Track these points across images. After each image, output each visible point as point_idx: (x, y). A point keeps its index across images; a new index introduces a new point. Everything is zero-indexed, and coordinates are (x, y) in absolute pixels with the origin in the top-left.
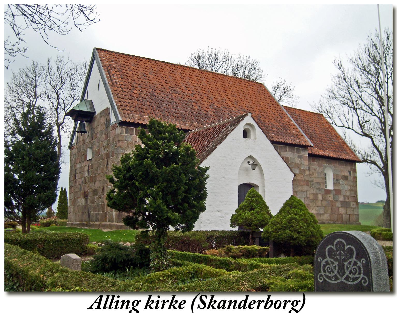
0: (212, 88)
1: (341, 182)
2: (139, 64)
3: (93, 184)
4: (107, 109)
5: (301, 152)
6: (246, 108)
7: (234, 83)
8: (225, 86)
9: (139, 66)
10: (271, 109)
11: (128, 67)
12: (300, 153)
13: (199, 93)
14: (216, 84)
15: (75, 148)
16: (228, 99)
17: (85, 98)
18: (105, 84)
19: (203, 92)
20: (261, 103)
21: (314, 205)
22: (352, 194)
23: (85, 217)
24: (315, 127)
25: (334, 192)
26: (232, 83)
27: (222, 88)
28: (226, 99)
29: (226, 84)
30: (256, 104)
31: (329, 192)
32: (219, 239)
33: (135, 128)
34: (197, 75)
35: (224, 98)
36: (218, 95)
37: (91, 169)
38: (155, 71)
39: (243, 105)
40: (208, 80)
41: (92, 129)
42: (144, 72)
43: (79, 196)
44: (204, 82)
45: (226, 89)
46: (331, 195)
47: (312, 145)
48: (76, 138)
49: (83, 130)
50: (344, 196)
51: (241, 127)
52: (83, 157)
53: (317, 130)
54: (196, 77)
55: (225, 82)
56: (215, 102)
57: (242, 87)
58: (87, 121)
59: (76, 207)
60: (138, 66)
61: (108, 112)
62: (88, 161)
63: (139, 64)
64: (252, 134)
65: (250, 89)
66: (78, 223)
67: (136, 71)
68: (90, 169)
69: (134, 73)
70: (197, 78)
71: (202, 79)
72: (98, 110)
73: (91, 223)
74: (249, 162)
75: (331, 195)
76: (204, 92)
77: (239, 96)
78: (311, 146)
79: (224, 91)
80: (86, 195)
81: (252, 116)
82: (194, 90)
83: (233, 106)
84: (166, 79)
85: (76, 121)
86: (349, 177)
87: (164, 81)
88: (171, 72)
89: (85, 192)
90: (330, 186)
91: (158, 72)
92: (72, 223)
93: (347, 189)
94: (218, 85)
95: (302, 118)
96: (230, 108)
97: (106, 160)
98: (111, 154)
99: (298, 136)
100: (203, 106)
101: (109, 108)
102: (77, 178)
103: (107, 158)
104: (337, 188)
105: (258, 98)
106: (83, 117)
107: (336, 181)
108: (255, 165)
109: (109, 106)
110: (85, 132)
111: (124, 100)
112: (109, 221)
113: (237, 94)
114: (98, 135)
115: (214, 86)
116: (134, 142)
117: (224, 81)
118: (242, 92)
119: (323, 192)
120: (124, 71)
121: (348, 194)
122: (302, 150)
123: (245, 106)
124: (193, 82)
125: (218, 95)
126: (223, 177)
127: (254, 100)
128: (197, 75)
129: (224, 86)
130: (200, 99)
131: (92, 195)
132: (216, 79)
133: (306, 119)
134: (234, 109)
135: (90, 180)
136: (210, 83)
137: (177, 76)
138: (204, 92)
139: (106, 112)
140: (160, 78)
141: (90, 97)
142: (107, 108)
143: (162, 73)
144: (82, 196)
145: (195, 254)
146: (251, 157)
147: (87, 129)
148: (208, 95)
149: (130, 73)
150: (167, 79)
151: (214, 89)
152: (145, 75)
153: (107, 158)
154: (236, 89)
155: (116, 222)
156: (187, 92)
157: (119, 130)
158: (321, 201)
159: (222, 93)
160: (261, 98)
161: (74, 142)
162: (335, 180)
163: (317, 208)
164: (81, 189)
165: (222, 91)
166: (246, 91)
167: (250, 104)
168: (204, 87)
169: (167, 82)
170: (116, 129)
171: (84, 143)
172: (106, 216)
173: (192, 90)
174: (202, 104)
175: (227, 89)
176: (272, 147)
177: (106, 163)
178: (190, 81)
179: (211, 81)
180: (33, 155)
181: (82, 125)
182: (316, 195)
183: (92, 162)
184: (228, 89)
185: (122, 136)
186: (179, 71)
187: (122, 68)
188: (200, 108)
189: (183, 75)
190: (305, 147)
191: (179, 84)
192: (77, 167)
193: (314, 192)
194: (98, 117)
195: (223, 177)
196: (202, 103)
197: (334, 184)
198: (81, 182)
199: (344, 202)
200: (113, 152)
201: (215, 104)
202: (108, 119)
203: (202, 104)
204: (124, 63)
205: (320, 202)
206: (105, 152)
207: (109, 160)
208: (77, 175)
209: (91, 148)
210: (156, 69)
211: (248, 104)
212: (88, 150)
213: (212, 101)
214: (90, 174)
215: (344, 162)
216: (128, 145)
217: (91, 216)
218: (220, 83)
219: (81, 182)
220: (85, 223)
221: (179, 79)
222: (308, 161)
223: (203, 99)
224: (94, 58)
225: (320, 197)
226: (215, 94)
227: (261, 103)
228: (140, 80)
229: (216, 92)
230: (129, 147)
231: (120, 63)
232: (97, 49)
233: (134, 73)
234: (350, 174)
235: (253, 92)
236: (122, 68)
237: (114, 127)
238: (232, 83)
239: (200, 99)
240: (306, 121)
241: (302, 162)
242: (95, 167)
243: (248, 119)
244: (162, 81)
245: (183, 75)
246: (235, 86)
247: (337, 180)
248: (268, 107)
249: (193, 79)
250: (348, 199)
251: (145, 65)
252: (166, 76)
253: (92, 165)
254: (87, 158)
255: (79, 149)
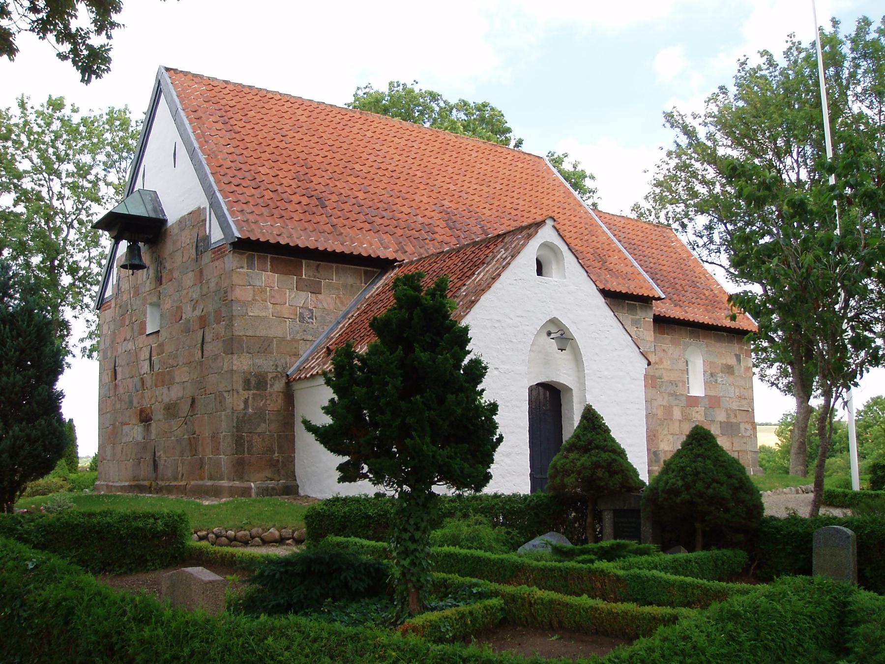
0: (434, 166)
1: (720, 380)
2: (266, 106)
3: (165, 390)
4: (199, 211)
5: (639, 311)
6: (514, 212)
7: (482, 156)
8: (462, 162)
9: (267, 111)
10: (568, 214)
11: (241, 112)
12: (636, 314)
13: (407, 177)
14: (443, 157)
15: (113, 305)
16: (471, 191)
17: (138, 186)
18: (192, 154)
19: (417, 173)
20: (544, 201)
21: (665, 432)
22: (743, 406)
23: (145, 470)
24: (659, 256)
25: (706, 402)
26: (476, 154)
27: (457, 165)
28: (469, 190)
29: (463, 156)
30: (533, 202)
31: (693, 401)
32: (507, 509)
33: (269, 256)
34: (398, 135)
35: (462, 189)
36: (449, 181)
37: (158, 354)
38: (304, 124)
39: (505, 204)
40: (423, 147)
41: (159, 262)
42: (279, 126)
43: (127, 420)
44: (416, 151)
45: (464, 168)
46: (701, 409)
47: (663, 296)
48: (115, 282)
49: (136, 262)
50: (727, 410)
51: (530, 252)
52: (136, 327)
53: (664, 262)
54: (396, 140)
55: (462, 150)
56: (446, 197)
57: (500, 165)
58: (146, 242)
59: (120, 447)
60: (264, 111)
61: (203, 218)
62: (151, 336)
63: (266, 106)
64: (553, 269)
65: (516, 168)
66: (127, 484)
67: (262, 122)
68: (154, 353)
69: (257, 127)
70: (400, 141)
71: (410, 144)
72: (173, 213)
73: (162, 483)
74: (549, 334)
75: (701, 409)
76: (419, 174)
77: (495, 185)
78: (659, 299)
79: (462, 172)
80: (145, 418)
81: (554, 227)
82: (395, 168)
83: (484, 205)
84: (330, 142)
85: (117, 240)
86: (736, 368)
87: (327, 148)
88: (340, 127)
89: (142, 411)
90: (697, 389)
91: (311, 126)
92: (111, 484)
93: (732, 395)
94: (447, 158)
95: (629, 236)
96: (478, 210)
97: (200, 333)
98: (212, 318)
99: (631, 276)
100: (420, 205)
101: (205, 209)
102: (119, 377)
103: (203, 327)
104: (712, 393)
105: (537, 189)
106: (139, 230)
107: (711, 377)
108: (562, 337)
109: (205, 203)
110: (142, 267)
111: (239, 190)
112: (211, 479)
113: (490, 179)
114: (176, 274)
115: (439, 161)
116: (268, 289)
117: (459, 150)
118: (500, 175)
119: (683, 402)
120: (233, 122)
121: (735, 406)
122: (641, 308)
123: (511, 206)
124: (392, 151)
125: (449, 181)
126: (497, 369)
127: (529, 193)
128: (398, 135)
129: (460, 162)
130: (411, 190)
131: (161, 417)
132: (440, 145)
133: (639, 238)
134: (488, 213)
135: (157, 380)
136: (428, 153)
137: (355, 136)
138: (419, 174)
139: (196, 219)
140: (318, 140)
141: (149, 181)
142: (199, 208)
143: (321, 129)
144: (135, 420)
145: (599, 544)
146: (554, 321)
147: (146, 258)
148: (428, 181)
149: (248, 126)
150: (333, 143)
151: (440, 167)
152: (283, 132)
153: (203, 327)
154: (486, 167)
155: (229, 479)
156: (380, 172)
157: (231, 261)
158: (680, 421)
159: (457, 177)
160: (542, 190)
161: (108, 293)
162: (708, 373)
163: (670, 437)
164: (131, 402)
165: (456, 171)
166: (508, 173)
167: (521, 202)
168: (417, 162)
169: (334, 149)
170: (226, 259)
171: (137, 293)
172: (201, 467)
173: (391, 168)
174: (417, 200)
175: (467, 168)
176: (600, 300)
177: (200, 341)
178: (385, 148)
179: (430, 148)
180: (833, 188)
181: (133, 250)
182: (668, 409)
183: (161, 339)
184: (470, 169)
185: (239, 273)
186: (358, 126)
187: (230, 114)
188: (413, 212)
189: (369, 134)
190: (645, 301)
191: (361, 155)
192: (119, 350)
193: (665, 403)
194: (176, 231)
195: (497, 369)
196: (418, 198)
197: (706, 383)
198: (131, 386)
199: (727, 423)
200: (218, 312)
201: (446, 203)
202: (201, 235)
203: (417, 200)
204: (232, 103)
205: (677, 424)
206: (198, 313)
207: (206, 333)
208: (119, 370)
209: (156, 305)
210: (306, 119)
211: (516, 202)
212: (149, 309)
213: (438, 195)
214: (156, 368)
215: (725, 334)
216: (254, 296)
217: (160, 467)
218: (451, 154)
219: (131, 386)
220: (147, 483)
221: (360, 143)
222: (652, 333)
223: (417, 191)
224: (161, 91)
225: (677, 414)
226: (443, 179)
227: (544, 201)
228: (273, 144)
229: (445, 174)
230: (256, 300)
231: (223, 102)
232: (168, 69)
233: (257, 127)
234: (739, 360)
235: (525, 177)
236: (230, 114)
237: (219, 251)
238: (476, 154)
239: (411, 190)
240: (639, 243)
241: (641, 334)
242: (168, 349)
243: (547, 234)
244: (322, 147)
245: (369, 134)
246: (484, 160)
247: (712, 375)
248: (560, 210)
249: (391, 144)
250: (736, 416)
251: (280, 108)
252: (330, 136)
253: (161, 345)
254: (145, 329)
255: (124, 310)
